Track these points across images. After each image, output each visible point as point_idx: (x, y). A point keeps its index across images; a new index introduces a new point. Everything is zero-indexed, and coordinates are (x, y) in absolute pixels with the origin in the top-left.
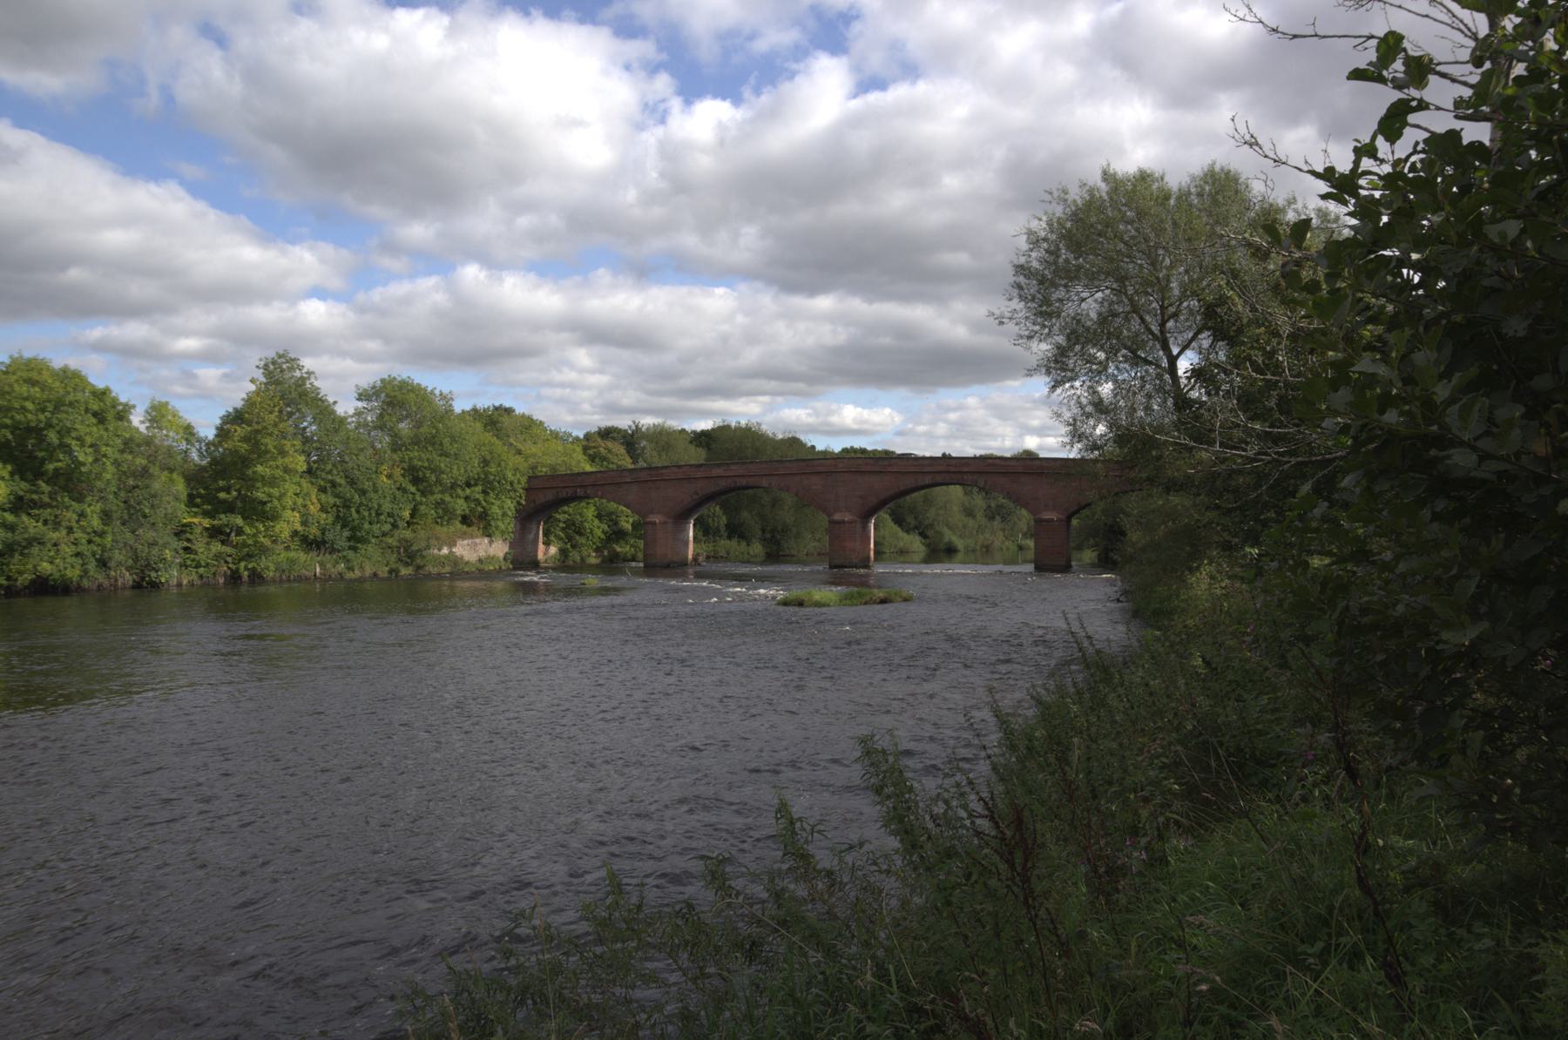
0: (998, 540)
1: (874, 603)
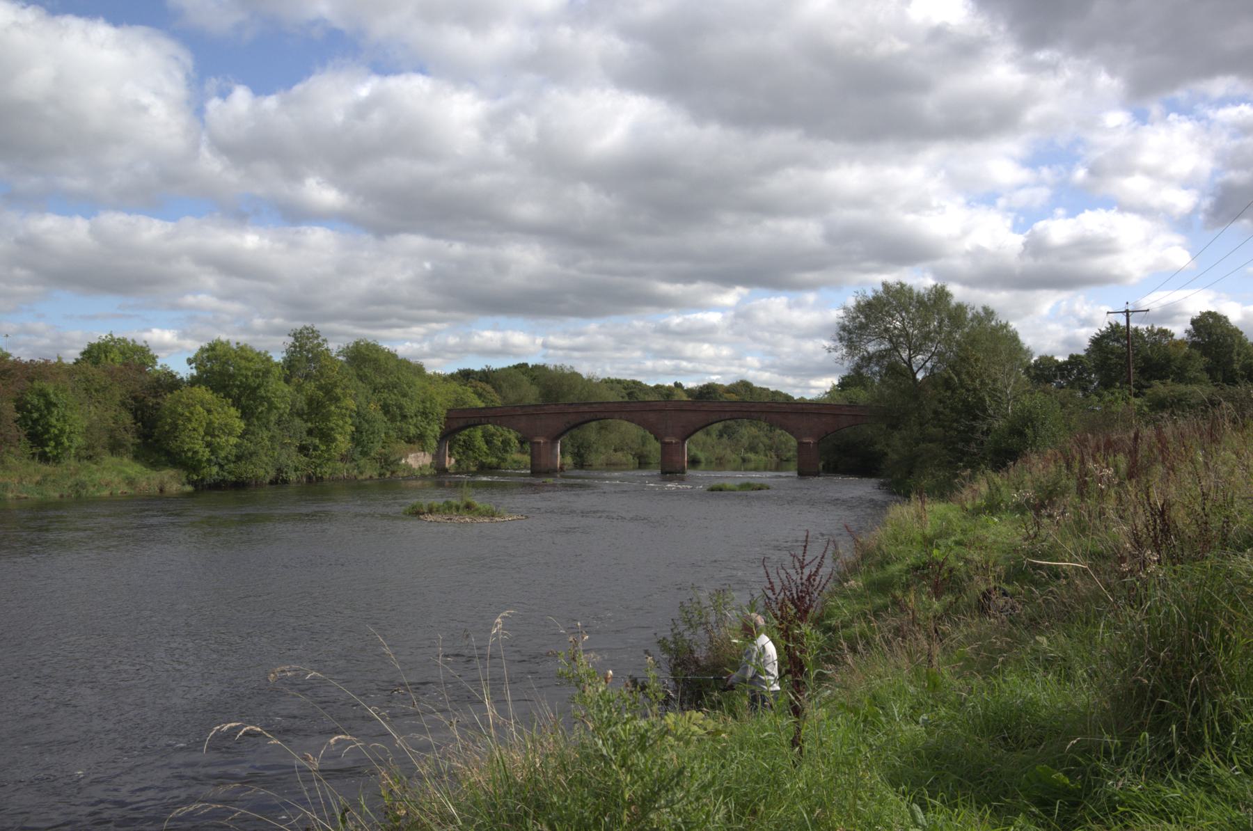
0: (729, 454)
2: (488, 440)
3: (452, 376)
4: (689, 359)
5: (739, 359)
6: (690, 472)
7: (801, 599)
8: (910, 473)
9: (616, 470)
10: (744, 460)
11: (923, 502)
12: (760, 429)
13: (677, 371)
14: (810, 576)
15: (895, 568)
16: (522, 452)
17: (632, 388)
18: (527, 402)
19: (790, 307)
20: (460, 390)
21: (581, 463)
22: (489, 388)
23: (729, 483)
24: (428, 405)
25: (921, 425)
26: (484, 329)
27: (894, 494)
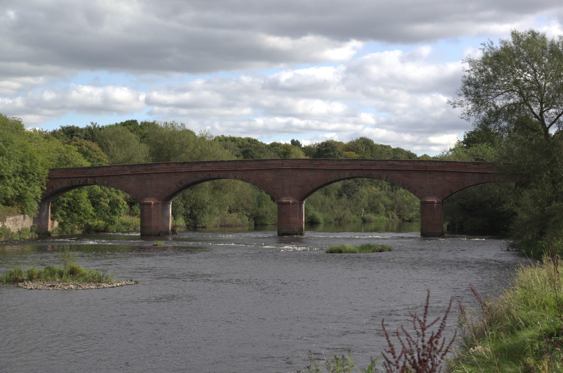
0: (349, 215)
1: (377, 252)
2: (95, 202)
3: (54, 133)
4: (302, 116)
5: (355, 116)
6: (307, 234)
7: (423, 362)
8: (542, 234)
9: (230, 232)
10: (364, 221)
11: (556, 265)
12: (382, 188)
13: (288, 128)
14: (432, 339)
15: (526, 335)
16: (131, 213)
17: (248, 149)
18: (136, 161)
19: (403, 60)
20: (63, 149)
21: (194, 224)
22: (95, 146)
23: (349, 245)
24: (28, 164)
25: (554, 183)
26: (84, 84)
27: (523, 255)
